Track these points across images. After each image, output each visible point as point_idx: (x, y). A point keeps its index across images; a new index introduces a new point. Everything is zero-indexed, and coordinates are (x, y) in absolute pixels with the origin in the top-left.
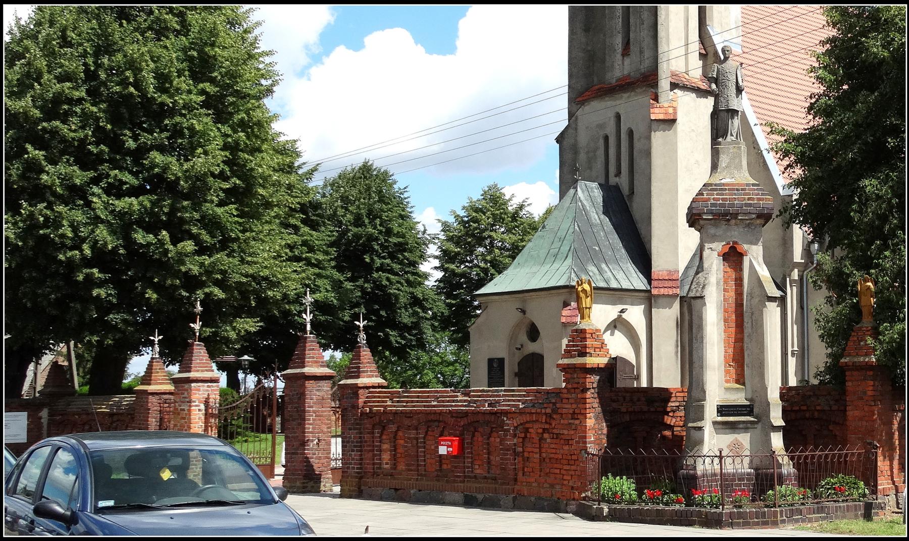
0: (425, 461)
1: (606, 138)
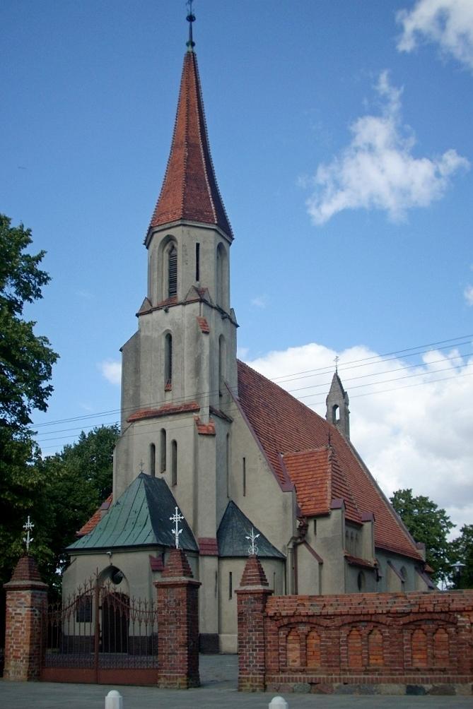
0: (347, 657)
1: (153, 446)
